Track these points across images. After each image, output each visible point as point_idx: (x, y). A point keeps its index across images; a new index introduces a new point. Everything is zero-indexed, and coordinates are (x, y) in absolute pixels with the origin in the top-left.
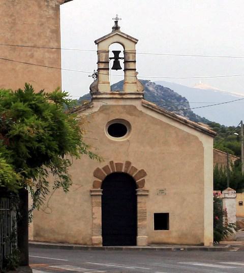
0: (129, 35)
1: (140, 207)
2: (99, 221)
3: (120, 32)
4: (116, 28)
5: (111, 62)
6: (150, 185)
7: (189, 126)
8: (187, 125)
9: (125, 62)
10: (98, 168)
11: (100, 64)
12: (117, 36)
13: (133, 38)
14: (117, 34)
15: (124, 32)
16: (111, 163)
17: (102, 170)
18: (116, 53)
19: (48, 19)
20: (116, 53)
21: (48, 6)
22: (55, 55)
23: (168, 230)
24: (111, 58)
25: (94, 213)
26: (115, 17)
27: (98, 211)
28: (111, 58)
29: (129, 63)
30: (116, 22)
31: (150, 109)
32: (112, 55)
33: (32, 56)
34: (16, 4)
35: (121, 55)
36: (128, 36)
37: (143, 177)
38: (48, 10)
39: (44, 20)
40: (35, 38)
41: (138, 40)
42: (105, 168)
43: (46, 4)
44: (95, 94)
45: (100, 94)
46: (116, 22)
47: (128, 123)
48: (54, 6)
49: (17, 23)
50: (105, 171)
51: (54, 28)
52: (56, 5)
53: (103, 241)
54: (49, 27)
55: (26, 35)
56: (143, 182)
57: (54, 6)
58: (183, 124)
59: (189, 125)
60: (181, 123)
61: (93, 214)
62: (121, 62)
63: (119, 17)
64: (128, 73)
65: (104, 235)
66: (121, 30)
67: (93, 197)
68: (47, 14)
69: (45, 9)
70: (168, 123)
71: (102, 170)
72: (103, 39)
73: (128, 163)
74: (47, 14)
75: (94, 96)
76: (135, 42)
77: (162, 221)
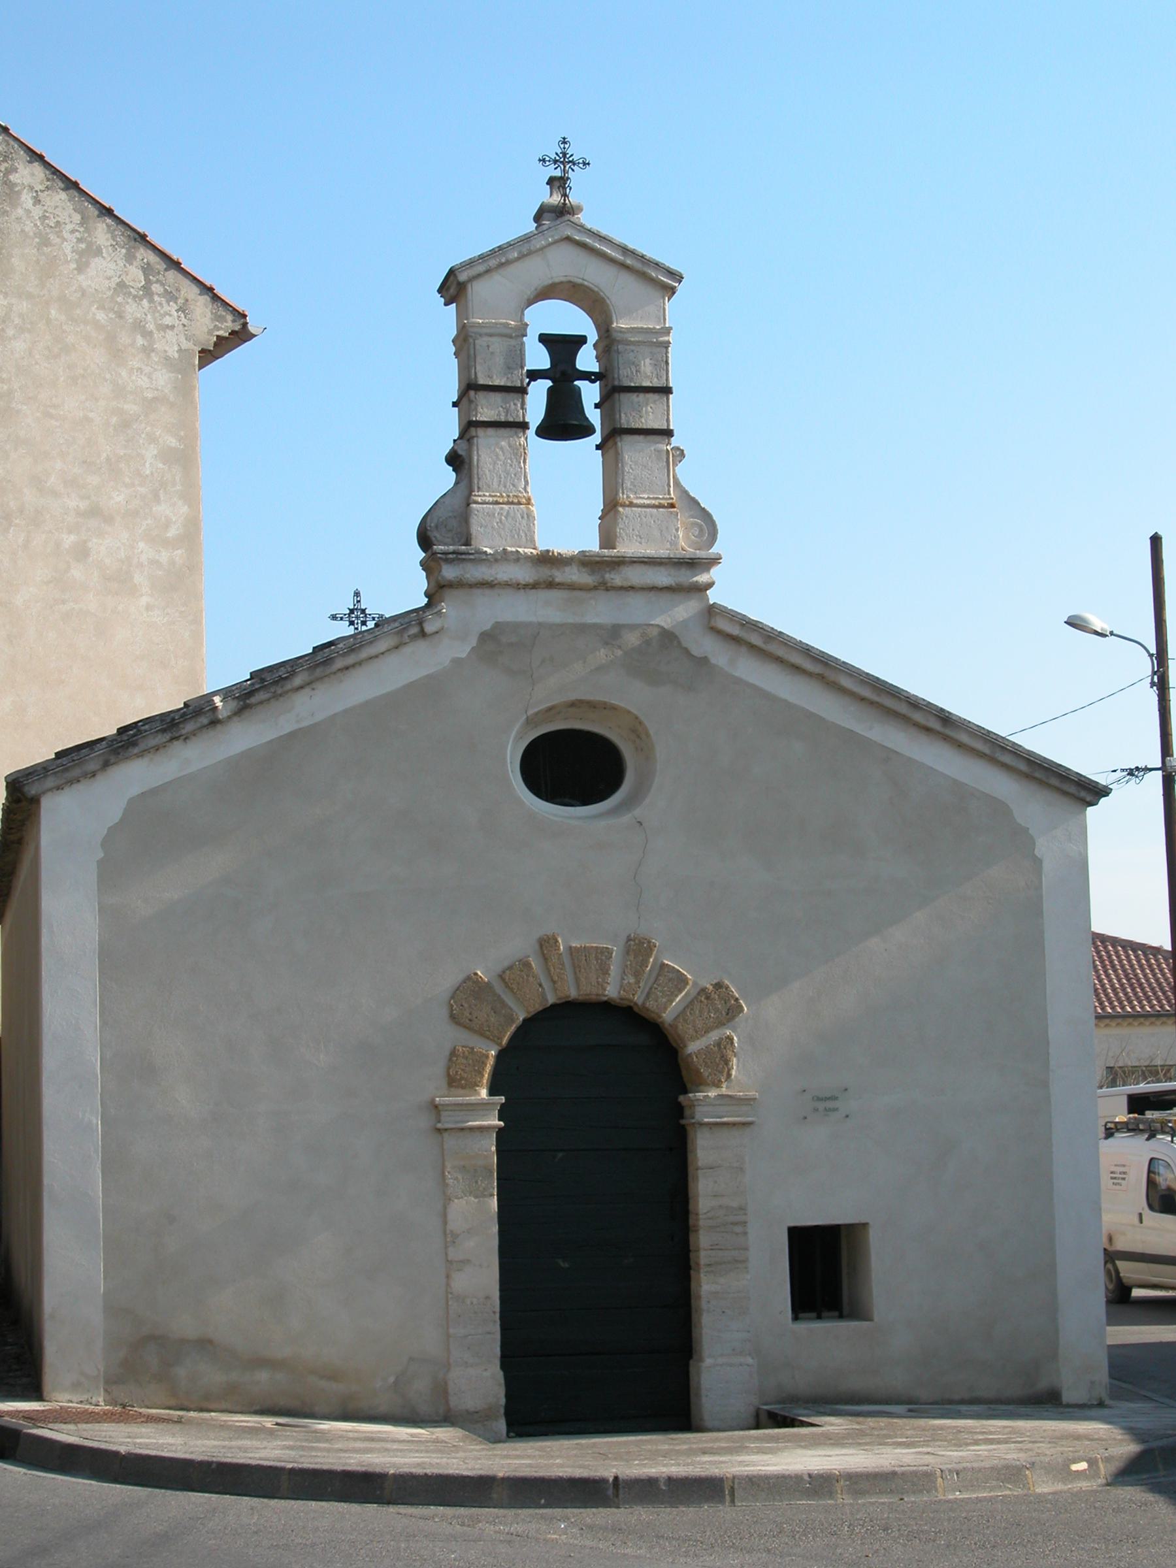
0: (631, 246)
1: (707, 1194)
2: (481, 1277)
3: (582, 228)
4: (555, 214)
5: (538, 396)
6: (747, 1075)
7: (960, 745)
8: (946, 738)
9: (612, 393)
10: (472, 979)
11: (481, 398)
12: (568, 250)
13: (657, 265)
14: (568, 239)
15: (604, 232)
16: (546, 944)
17: (499, 988)
18: (563, 347)
19: (150, 405)
20: (563, 347)
21: (148, 350)
22: (179, 554)
23: (867, 1317)
24: (534, 375)
25: (455, 1236)
26: (553, 151)
27: (477, 1214)
28: (534, 375)
29: (634, 397)
30: (558, 183)
31: (752, 647)
32: (538, 358)
33: (82, 552)
34: (10, 332)
35: (587, 360)
36: (625, 250)
37: (721, 1024)
38: (147, 369)
39: (131, 408)
40: (94, 480)
41: (679, 278)
42: (514, 975)
43: (140, 341)
44: (457, 558)
45: (481, 558)
46: (558, 183)
47: (637, 730)
48: (173, 352)
49: (18, 412)
50: (576, 967)
51: (172, 442)
52: (180, 351)
53: (509, 1396)
54: (152, 439)
55: (59, 465)
56: (721, 1055)
57: (176, 355)
58: (928, 730)
59: (964, 738)
60: (916, 725)
61: (450, 1238)
62: (590, 393)
63: (575, 152)
64: (633, 453)
65: (513, 1357)
66: (582, 218)
67: (446, 1135)
68: (143, 382)
69: (135, 363)
70: (859, 728)
71: (499, 988)
72: (496, 260)
73: (639, 948)
74: (143, 382)
75: (449, 572)
76: (661, 281)
77: (823, 1269)
